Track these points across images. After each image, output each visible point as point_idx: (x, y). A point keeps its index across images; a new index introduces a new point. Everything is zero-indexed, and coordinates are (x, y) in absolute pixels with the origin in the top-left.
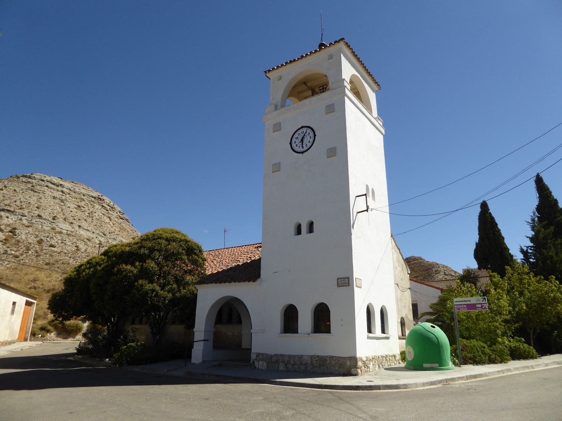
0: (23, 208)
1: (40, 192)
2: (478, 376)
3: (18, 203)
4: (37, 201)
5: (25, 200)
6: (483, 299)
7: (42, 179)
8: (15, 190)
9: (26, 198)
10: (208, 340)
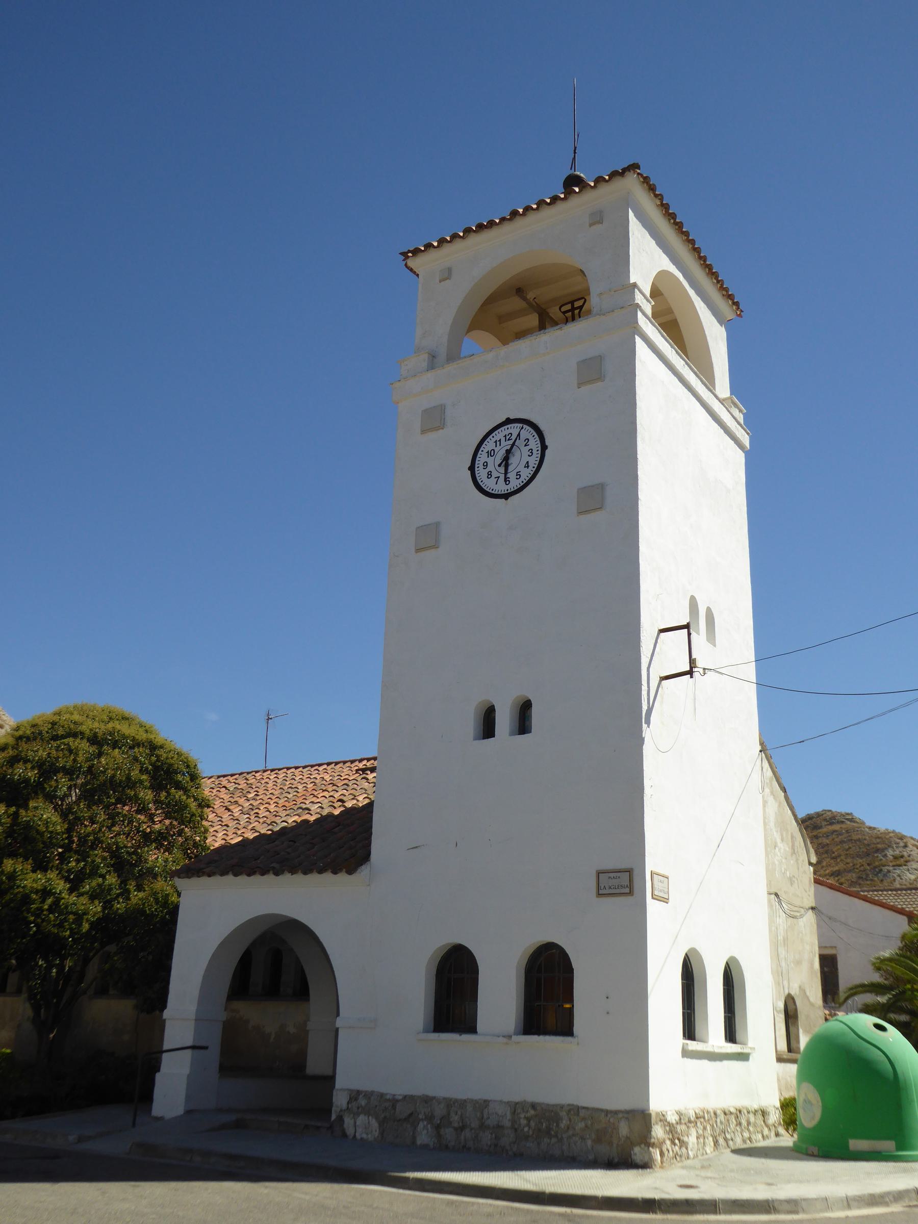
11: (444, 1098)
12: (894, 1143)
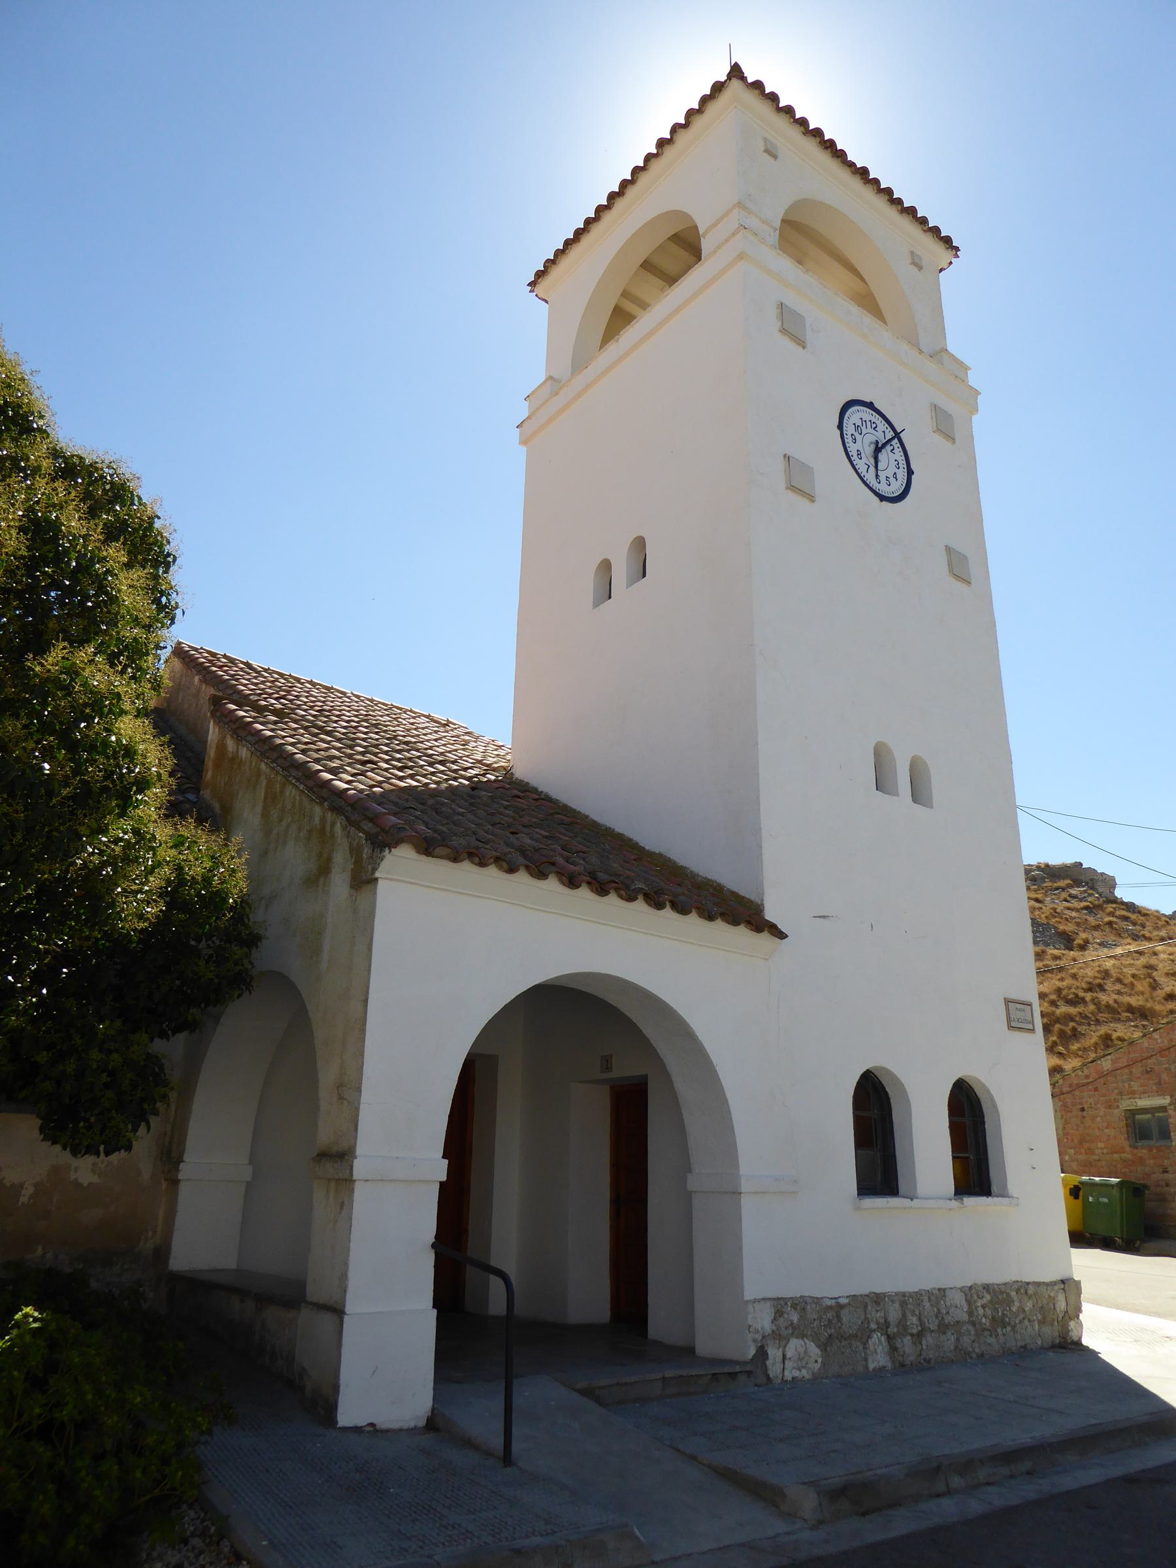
11: (897, 1294)
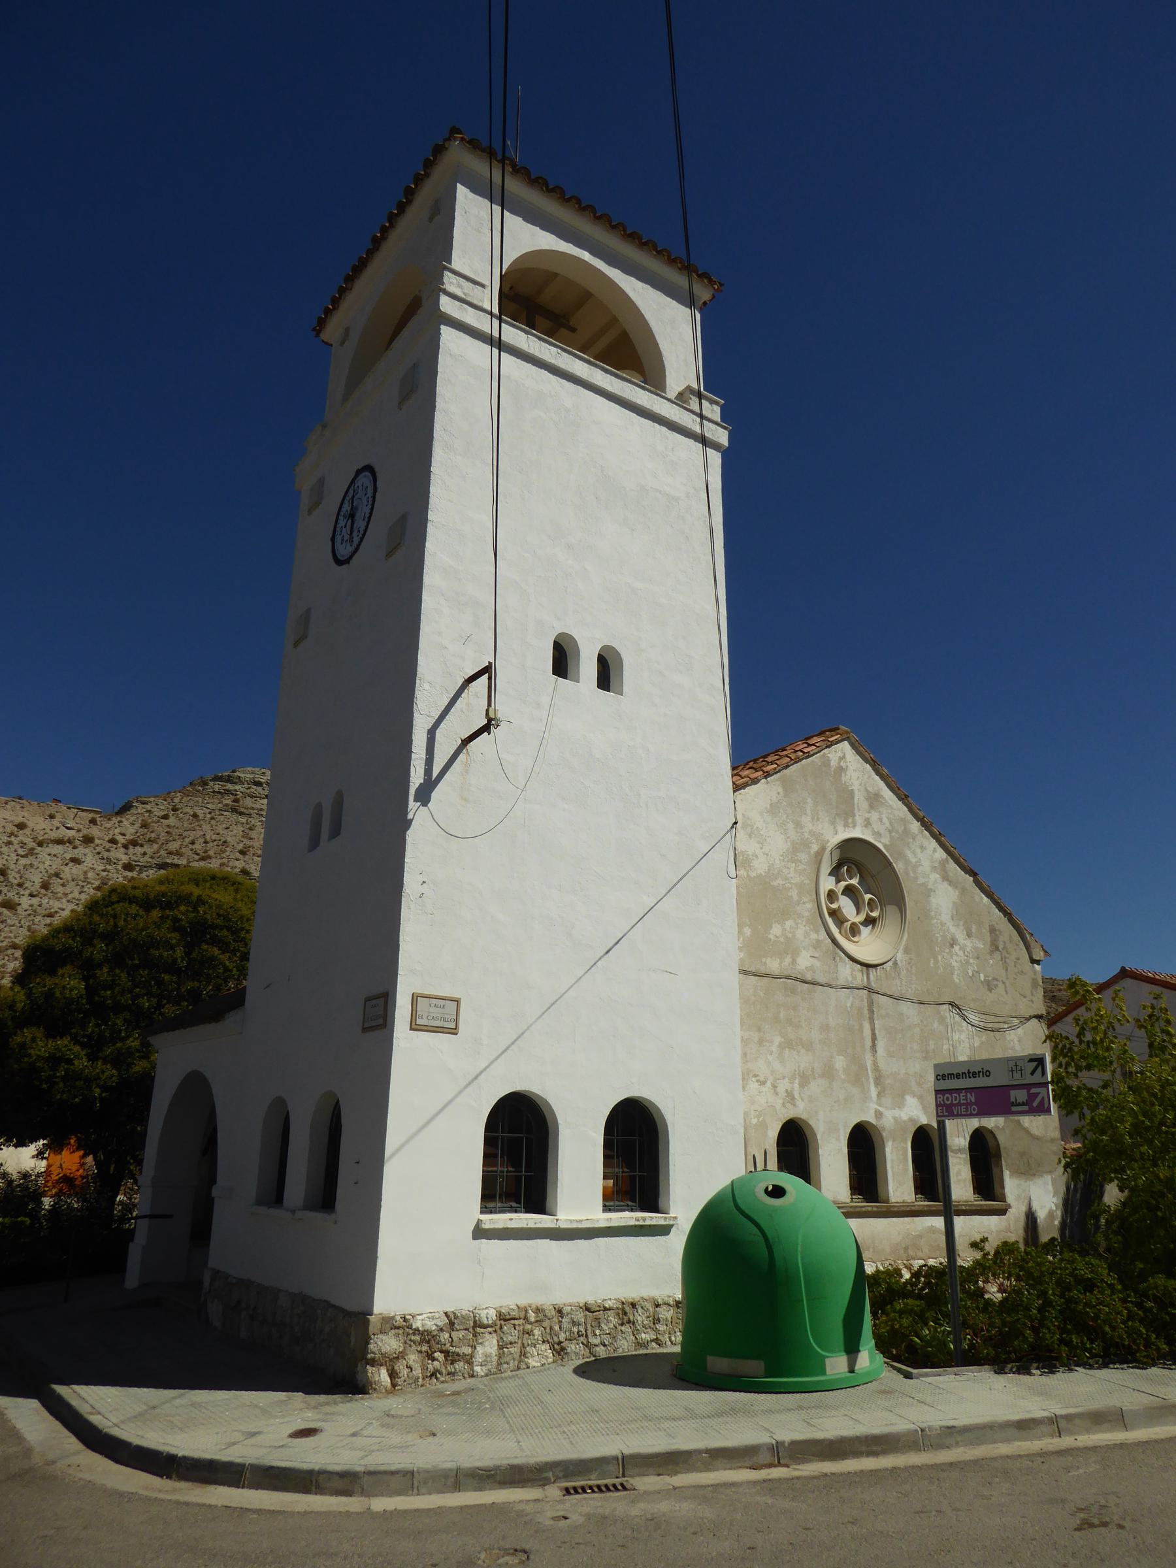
0: (210, 857)
1: (252, 812)
2: (864, 1448)
3: (198, 846)
4: (243, 837)
5: (217, 837)
6: (1035, 1064)
7: (256, 779)
8: (195, 816)
9: (217, 832)
10: (170, 1216)
12: (762, 1364)
